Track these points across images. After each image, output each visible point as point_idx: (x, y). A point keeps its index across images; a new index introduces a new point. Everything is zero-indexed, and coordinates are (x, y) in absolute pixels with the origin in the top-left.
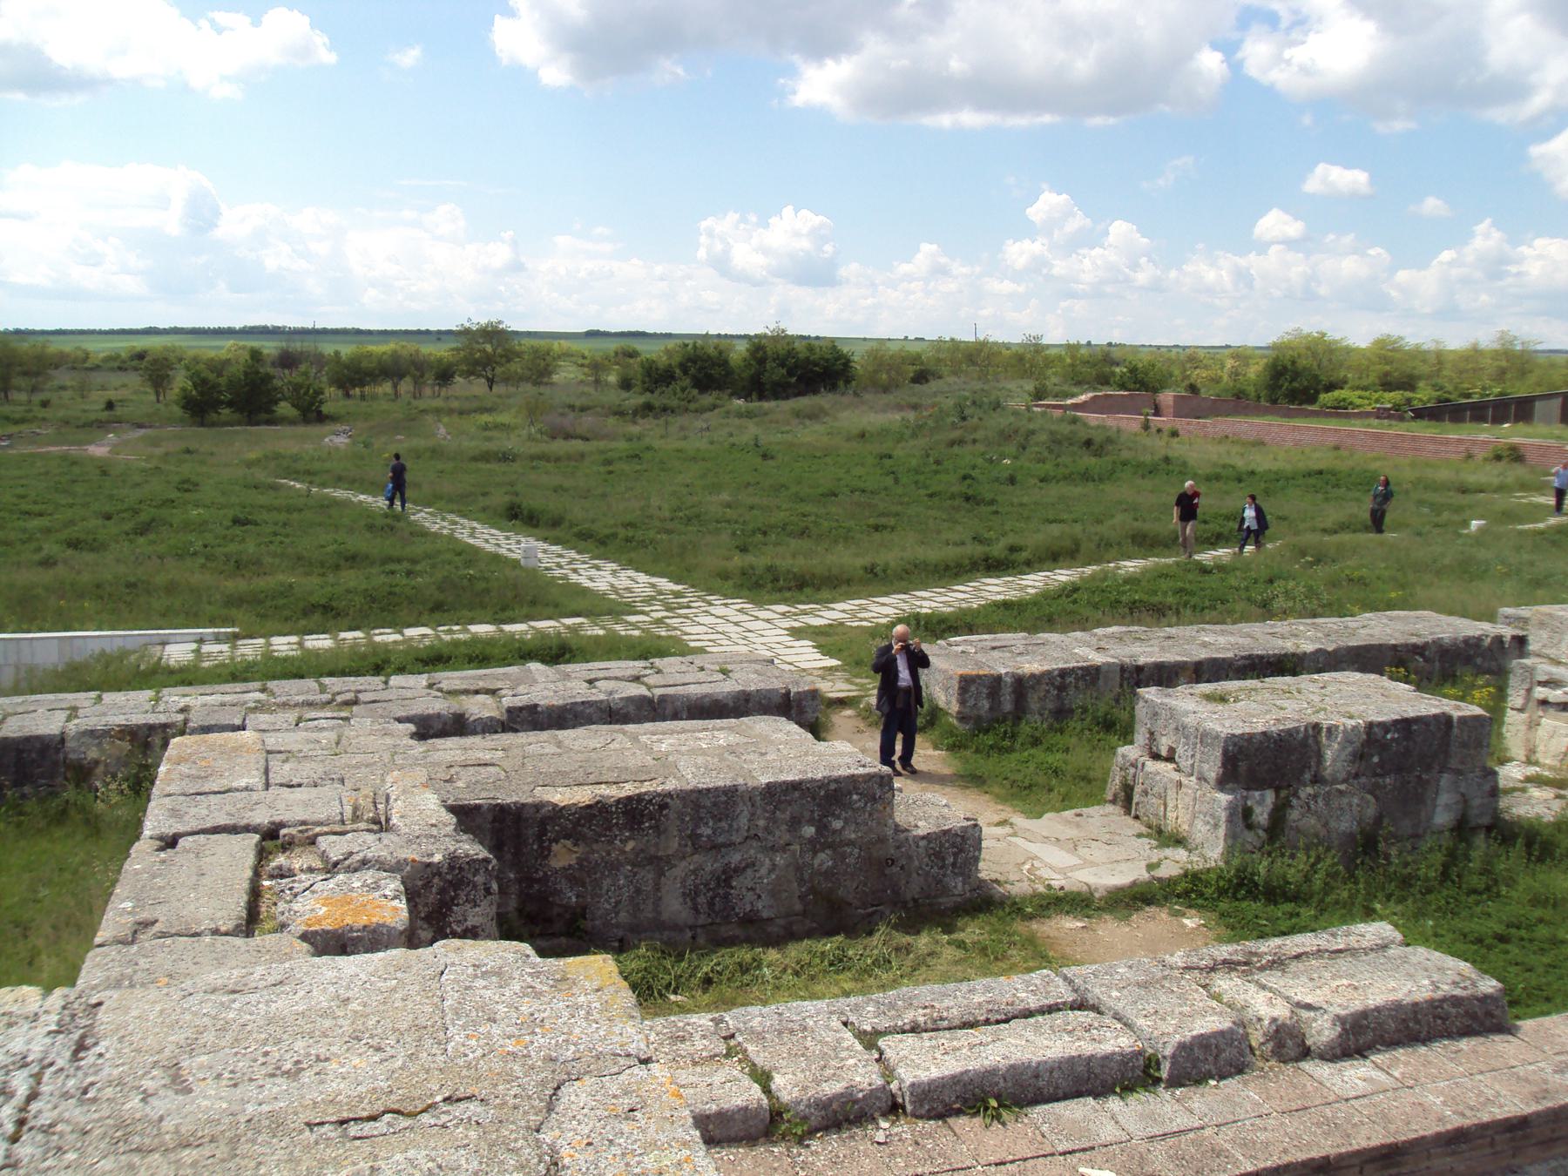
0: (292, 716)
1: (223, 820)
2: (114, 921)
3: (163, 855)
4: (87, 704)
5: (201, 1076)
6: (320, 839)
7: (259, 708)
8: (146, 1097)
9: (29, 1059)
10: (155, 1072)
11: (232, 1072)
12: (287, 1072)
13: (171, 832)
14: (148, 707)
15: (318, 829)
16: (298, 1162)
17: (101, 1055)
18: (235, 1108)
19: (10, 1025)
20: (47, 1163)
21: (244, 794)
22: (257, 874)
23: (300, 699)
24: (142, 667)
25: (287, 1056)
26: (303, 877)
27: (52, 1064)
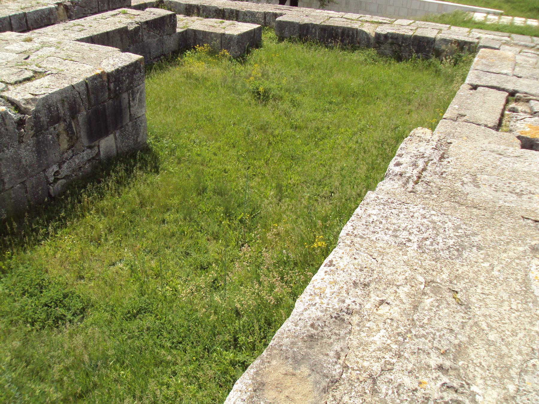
0: (518, 49)
1: (495, 84)
2: (451, 111)
3: (471, 91)
4: (446, 29)
5: (484, 183)
6: (532, 101)
7: (506, 43)
8: (463, 184)
9: (425, 156)
10: (467, 175)
11: (496, 185)
12: (516, 193)
13: (476, 84)
14: (466, 34)
15: (531, 97)
16: (517, 231)
17: (449, 162)
18: (495, 200)
19: (420, 141)
20: (426, 196)
21: (505, 76)
22: (504, 110)
23: (523, 43)
24: (465, 19)
25: (518, 187)
26: (522, 114)
27: (432, 160)
